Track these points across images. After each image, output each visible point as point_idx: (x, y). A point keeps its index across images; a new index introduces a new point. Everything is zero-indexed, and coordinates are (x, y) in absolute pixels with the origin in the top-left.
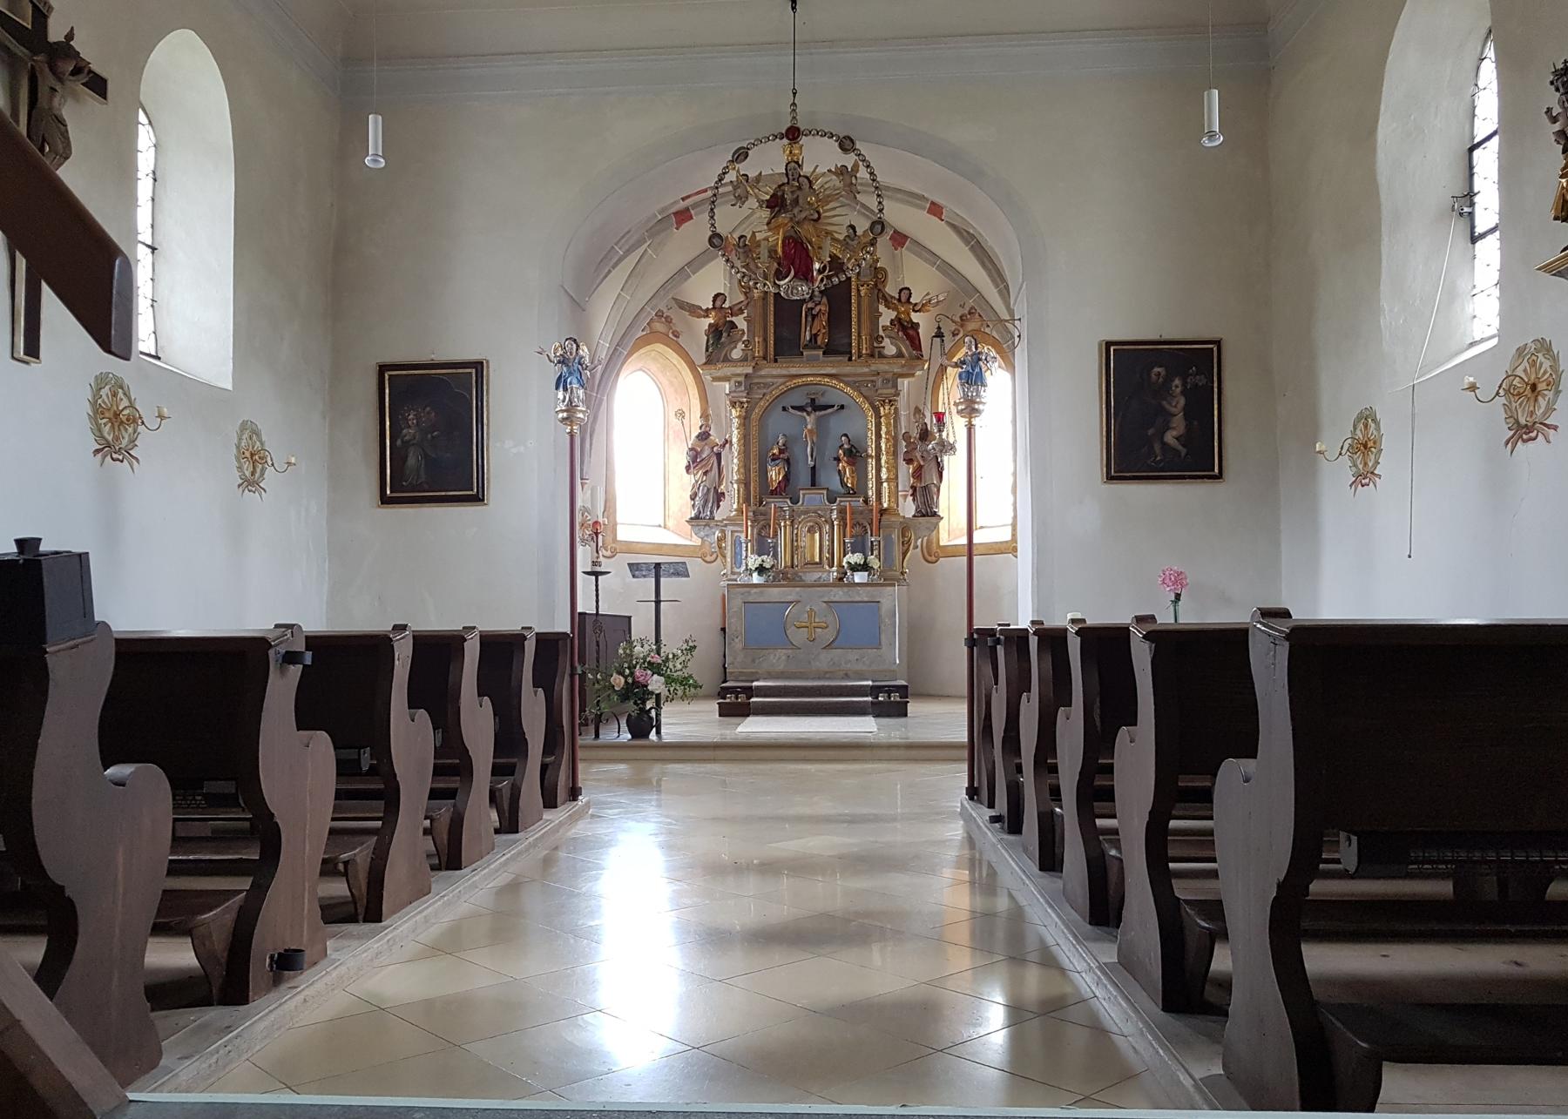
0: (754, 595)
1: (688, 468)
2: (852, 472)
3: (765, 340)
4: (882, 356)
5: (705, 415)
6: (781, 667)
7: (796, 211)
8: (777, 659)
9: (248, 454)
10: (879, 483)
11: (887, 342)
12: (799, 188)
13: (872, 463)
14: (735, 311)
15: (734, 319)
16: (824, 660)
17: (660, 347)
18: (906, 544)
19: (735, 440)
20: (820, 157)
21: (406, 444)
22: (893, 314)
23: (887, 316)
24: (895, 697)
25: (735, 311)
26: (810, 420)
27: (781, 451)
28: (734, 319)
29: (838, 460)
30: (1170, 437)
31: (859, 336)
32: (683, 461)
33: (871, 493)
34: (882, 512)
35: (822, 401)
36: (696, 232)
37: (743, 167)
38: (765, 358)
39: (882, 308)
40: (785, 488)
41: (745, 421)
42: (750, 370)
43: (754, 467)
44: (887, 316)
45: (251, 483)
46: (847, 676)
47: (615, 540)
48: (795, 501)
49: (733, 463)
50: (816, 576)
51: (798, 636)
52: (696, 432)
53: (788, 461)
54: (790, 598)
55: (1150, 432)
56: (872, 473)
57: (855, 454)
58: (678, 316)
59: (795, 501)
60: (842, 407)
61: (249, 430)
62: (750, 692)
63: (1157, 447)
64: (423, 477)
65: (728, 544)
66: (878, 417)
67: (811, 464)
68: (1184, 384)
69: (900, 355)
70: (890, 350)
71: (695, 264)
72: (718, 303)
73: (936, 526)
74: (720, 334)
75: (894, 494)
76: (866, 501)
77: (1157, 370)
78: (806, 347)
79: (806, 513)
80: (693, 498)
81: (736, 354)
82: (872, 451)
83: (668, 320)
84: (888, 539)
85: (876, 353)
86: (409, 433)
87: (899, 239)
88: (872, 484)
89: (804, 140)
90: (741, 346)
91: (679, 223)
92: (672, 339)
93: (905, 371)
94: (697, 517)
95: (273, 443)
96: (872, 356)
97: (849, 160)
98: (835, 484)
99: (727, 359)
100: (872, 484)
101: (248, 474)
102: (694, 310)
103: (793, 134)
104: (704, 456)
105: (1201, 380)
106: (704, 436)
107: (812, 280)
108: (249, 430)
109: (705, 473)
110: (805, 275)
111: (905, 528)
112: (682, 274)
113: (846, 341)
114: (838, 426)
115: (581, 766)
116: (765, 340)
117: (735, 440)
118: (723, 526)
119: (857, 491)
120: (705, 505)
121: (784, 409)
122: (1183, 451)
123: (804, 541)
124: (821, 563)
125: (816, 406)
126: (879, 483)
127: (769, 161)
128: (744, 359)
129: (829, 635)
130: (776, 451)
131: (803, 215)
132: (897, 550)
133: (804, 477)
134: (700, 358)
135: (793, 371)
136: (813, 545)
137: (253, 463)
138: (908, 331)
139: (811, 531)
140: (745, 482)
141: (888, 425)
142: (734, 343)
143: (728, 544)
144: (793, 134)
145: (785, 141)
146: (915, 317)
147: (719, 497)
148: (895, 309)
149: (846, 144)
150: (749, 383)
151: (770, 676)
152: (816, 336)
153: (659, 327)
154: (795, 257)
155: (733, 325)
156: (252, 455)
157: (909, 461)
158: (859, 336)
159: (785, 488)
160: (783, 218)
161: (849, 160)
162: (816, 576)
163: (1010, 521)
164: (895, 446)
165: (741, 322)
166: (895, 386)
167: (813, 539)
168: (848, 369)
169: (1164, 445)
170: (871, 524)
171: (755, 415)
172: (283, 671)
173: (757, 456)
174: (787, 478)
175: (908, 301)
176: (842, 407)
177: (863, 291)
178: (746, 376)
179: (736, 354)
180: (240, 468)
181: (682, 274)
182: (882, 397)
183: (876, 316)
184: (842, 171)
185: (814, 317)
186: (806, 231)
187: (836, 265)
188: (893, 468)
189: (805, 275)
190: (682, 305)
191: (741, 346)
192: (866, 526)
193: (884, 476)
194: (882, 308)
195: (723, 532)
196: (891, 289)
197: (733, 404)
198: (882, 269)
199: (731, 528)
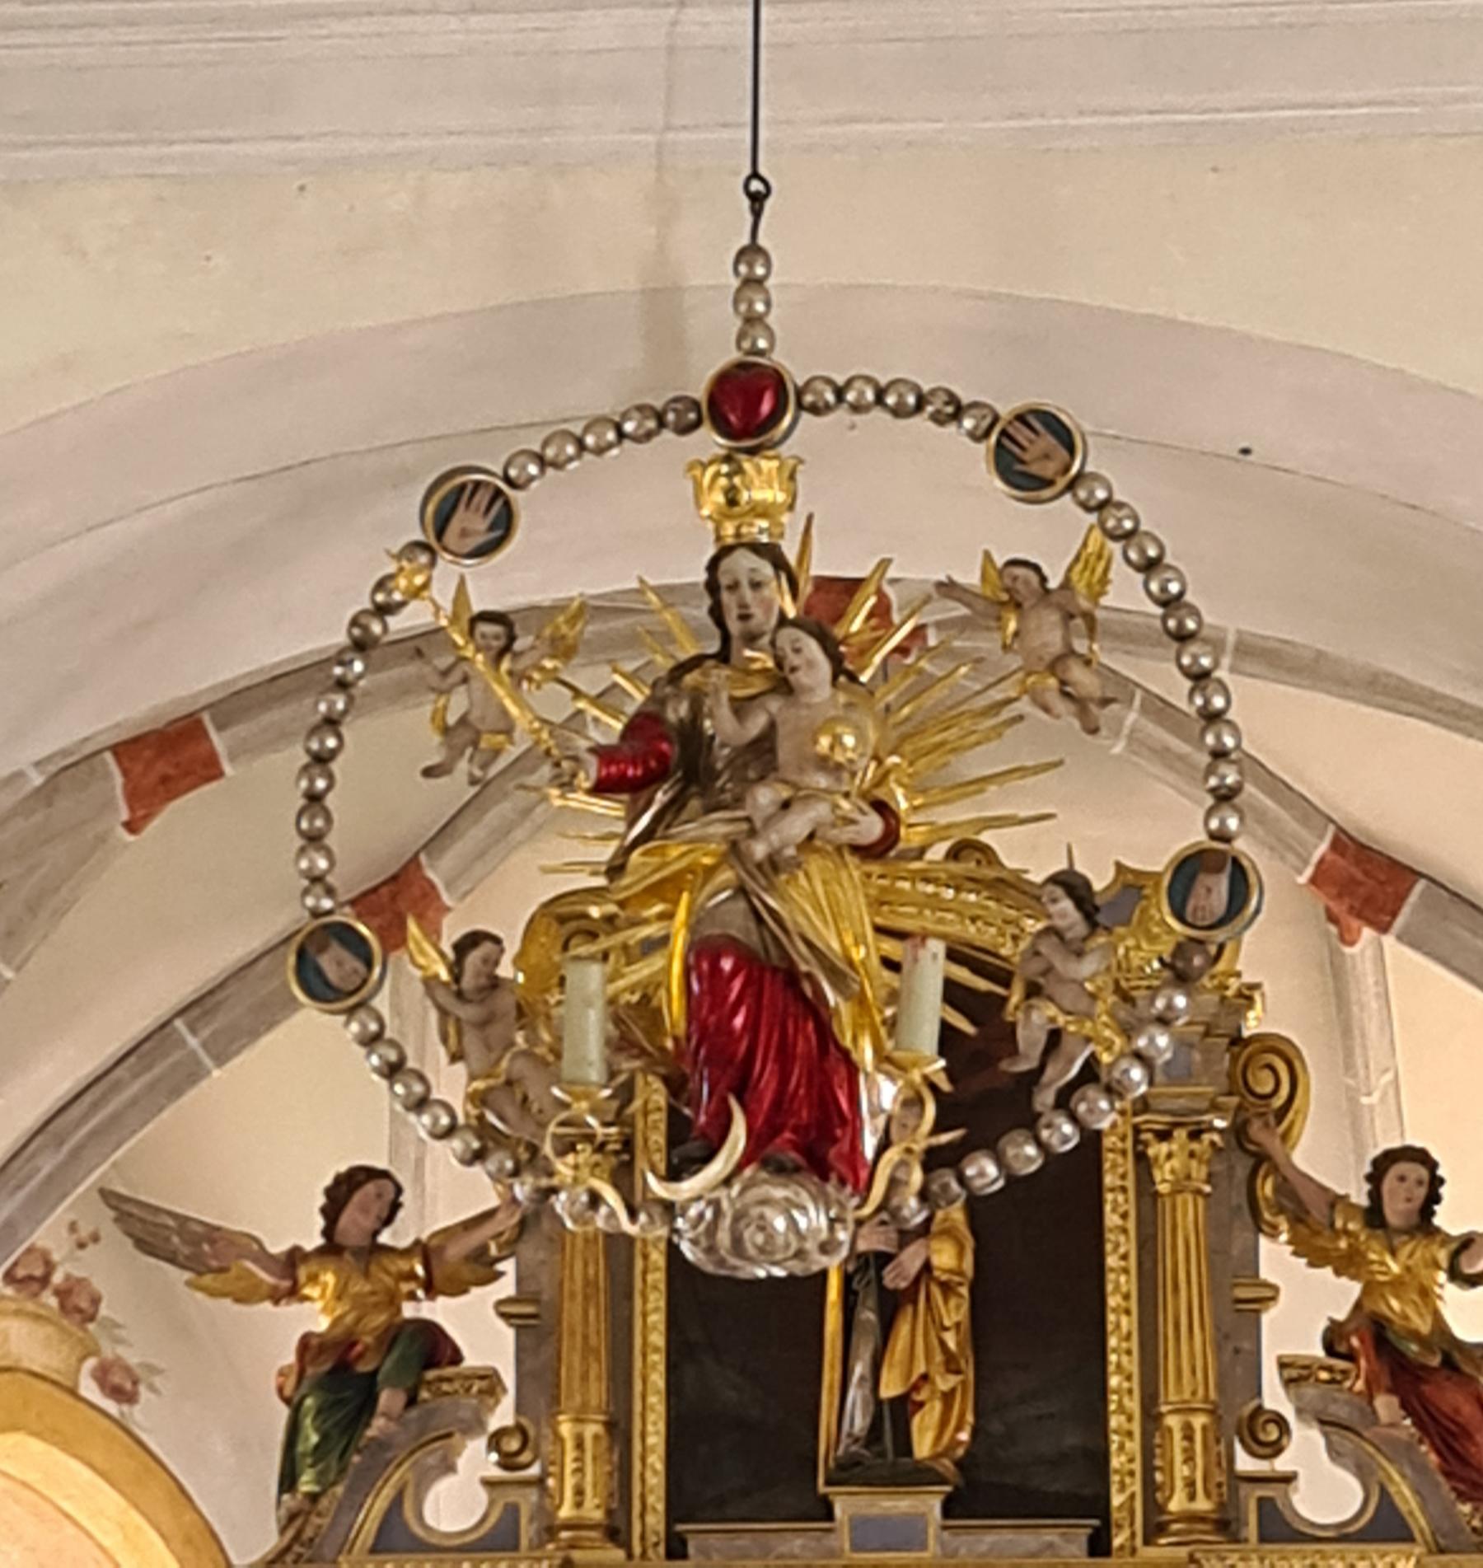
3: (619, 1430)
4: (1280, 1528)
7: (765, 797)
11: (1305, 1451)
12: (782, 683)
14: (449, 1265)
15: (439, 1310)
20: (894, 514)
22: (1337, 1296)
25: (449, 1265)
28: (439, 1310)
31: (1151, 1417)
36: (217, 879)
38: (615, 1532)
39: (1275, 1257)
44: (1303, 1304)
71: (221, 1015)
72: (353, 1221)
74: (364, 1395)
78: (849, 1472)
83: (77, 1305)
87: (1368, 883)
89: (804, 435)
90: (476, 1459)
91: (145, 801)
95: (612, 657)
96: (1225, 1525)
97: (1051, 535)
102: (200, 1252)
103: (746, 404)
107: (857, 1177)
110: (812, 1138)
112: (158, 1063)
113: (1072, 1439)
115: (959, 780)
116: (619, 1430)
127: (626, 536)
131: (797, 825)
142: (434, 1447)
144: (746, 404)
145: (709, 441)
148: (1348, 1264)
149: (1032, 452)
152: (903, 1408)
154: (754, 1053)
155: (434, 1347)
160: (702, 837)
161: (1051, 535)
163: (1324, 821)
165: (478, 1328)
175: (1423, 1221)
177: (1171, 1161)
181: (158, 1063)
183: (1241, 1307)
184: (1014, 590)
185: (891, 1306)
186: (829, 915)
187: (983, 1087)
189: (812, 1138)
190: (157, 1235)
191: (476, 1459)
194: (1275, 1257)
196: (1323, 1153)
198: (1277, 1048)
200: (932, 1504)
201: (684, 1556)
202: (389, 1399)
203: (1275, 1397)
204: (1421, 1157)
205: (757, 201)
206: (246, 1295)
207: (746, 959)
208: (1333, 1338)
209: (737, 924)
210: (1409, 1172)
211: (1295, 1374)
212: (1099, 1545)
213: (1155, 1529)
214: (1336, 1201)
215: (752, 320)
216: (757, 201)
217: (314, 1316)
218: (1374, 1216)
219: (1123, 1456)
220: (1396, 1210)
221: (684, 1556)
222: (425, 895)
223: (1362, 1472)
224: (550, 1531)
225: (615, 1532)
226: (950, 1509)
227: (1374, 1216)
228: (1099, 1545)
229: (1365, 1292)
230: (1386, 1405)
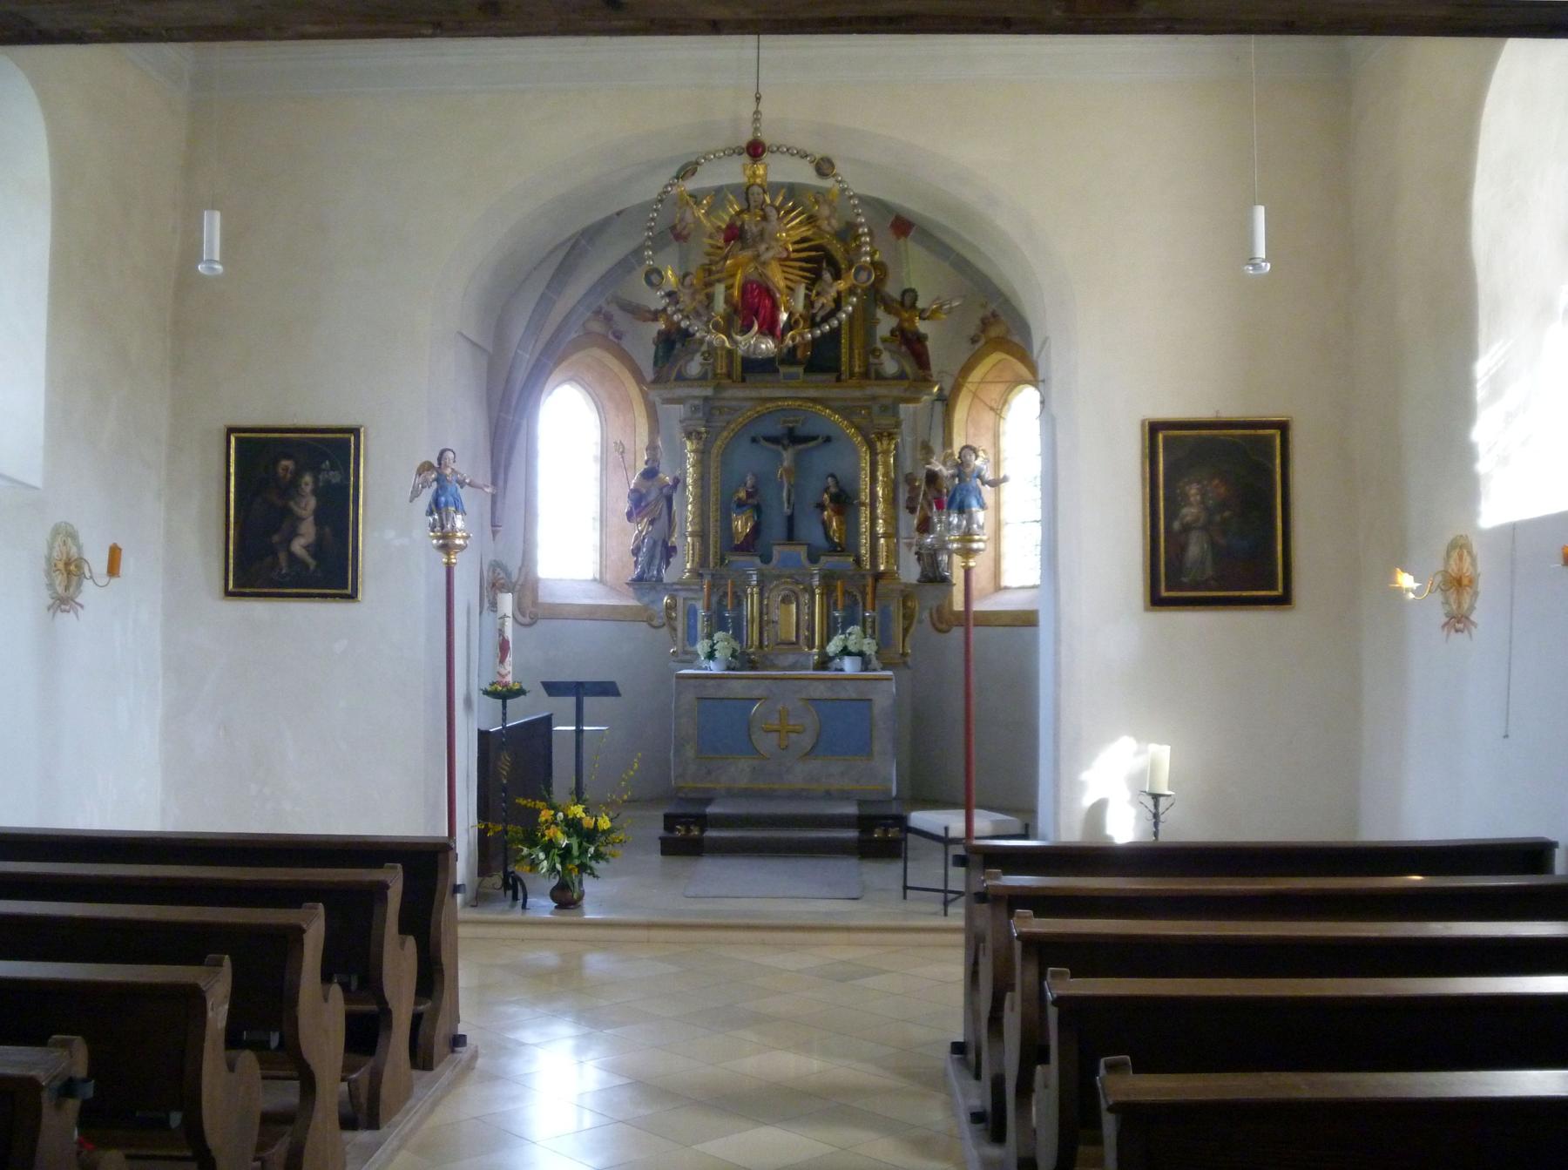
0: (711, 690)
1: (630, 515)
2: (840, 523)
4: (880, 377)
5: (652, 448)
6: (743, 783)
7: (763, 247)
8: (738, 772)
9: (61, 566)
10: (874, 537)
13: (865, 513)
14: (957, 551)
16: (799, 774)
17: (597, 352)
18: (908, 617)
19: (689, 480)
21: (1187, 528)
23: (886, 324)
24: (893, 833)
26: (788, 456)
27: (749, 495)
29: (821, 507)
30: (298, 546)
32: (625, 506)
33: (864, 551)
34: (878, 576)
35: (802, 430)
37: (690, 185)
38: (729, 375)
39: (880, 313)
40: (750, 544)
41: (703, 455)
42: (709, 392)
43: (713, 515)
44: (886, 324)
45: (63, 601)
46: (828, 795)
47: (535, 603)
48: (766, 559)
49: (687, 510)
50: (791, 659)
51: (766, 743)
52: (641, 467)
53: (758, 509)
54: (756, 693)
55: (276, 538)
56: (865, 525)
57: (844, 501)
58: (622, 320)
59: (766, 559)
60: (828, 440)
61: (64, 533)
62: (704, 821)
63: (282, 557)
64: (1209, 572)
65: (679, 615)
66: (874, 453)
67: (786, 510)
68: (316, 481)
69: (902, 376)
70: (890, 366)
73: (948, 595)
74: (672, 343)
75: (893, 554)
76: (858, 561)
77: (285, 463)
79: (778, 577)
80: (636, 551)
81: (694, 367)
82: (865, 497)
83: (608, 318)
84: (885, 614)
85: (871, 374)
86: (1190, 512)
88: (865, 540)
89: (766, 157)
90: (698, 358)
92: (614, 343)
93: (908, 394)
94: (640, 579)
96: (866, 375)
98: (817, 537)
99: (681, 378)
100: (865, 540)
101: (60, 590)
103: (755, 150)
104: (649, 500)
105: (335, 477)
106: (650, 474)
108: (64, 533)
109: (652, 522)
111: (906, 595)
114: (823, 462)
117: (689, 480)
118: (672, 590)
119: (845, 547)
120: (650, 563)
121: (754, 440)
122: (312, 563)
123: (776, 614)
124: (797, 643)
125: (793, 438)
126: (874, 537)
128: (703, 378)
129: (807, 741)
130: (742, 494)
132: (897, 627)
133: (776, 528)
134: (649, 374)
135: (765, 393)
136: (787, 618)
137: (66, 575)
138: (912, 345)
139: (786, 600)
140: (702, 535)
141: (886, 464)
143: (679, 615)
145: (746, 158)
146: (922, 326)
147: (669, 551)
148: (897, 314)
150: (709, 409)
151: (731, 794)
153: (597, 327)
156: (67, 564)
157: (912, 510)
158: (851, 349)
159: (750, 544)
162: (791, 659)
164: (895, 490)
166: (896, 414)
167: (789, 613)
168: (834, 392)
169: (292, 557)
170: (864, 594)
171: (714, 451)
172: (59, 1106)
173: (721, 499)
174: (756, 530)
175: (913, 306)
176: (828, 440)
178: (706, 399)
179: (694, 367)
180: (51, 585)
182: (877, 434)
188: (893, 521)
191: (698, 358)
192: (854, 591)
193: (880, 530)
194: (880, 313)
195: (673, 597)
196: (892, 289)
197: (689, 435)
199: (683, 594)
200: (800, 370)
201: (331, 573)
202: (678, 346)
203: (879, 345)
204: (913, 291)
205: (758, 99)
206: (645, 320)
207: (759, 286)
208: (892, 332)
209: (756, 277)
210: (909, 297)
211: (884, 341)
212: (838, 379)
213: (852, 375)
214: (893, 300)
215: (756, 129)
216: (758, 99)
217: (661, 325)
218: (902, 304)
219: (844, 358)
220: (908, 302)
221: (331, 573)
222: (1093, 1032)
223: (898, 362)
224: (715, 375)
225: (729, 375)
226: (805, 371)
227: (902, 304)
228: (838, 379)
229: (901, 321)
230: (904, 348)
